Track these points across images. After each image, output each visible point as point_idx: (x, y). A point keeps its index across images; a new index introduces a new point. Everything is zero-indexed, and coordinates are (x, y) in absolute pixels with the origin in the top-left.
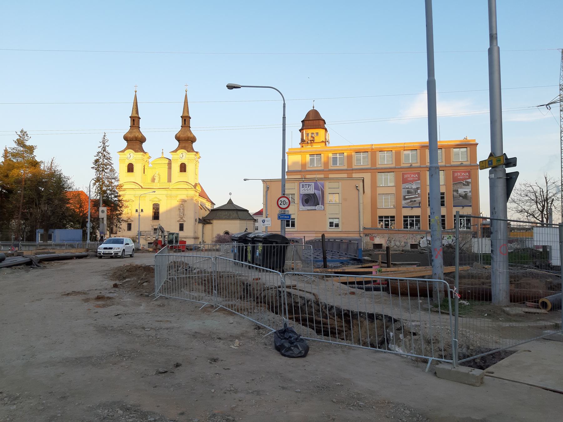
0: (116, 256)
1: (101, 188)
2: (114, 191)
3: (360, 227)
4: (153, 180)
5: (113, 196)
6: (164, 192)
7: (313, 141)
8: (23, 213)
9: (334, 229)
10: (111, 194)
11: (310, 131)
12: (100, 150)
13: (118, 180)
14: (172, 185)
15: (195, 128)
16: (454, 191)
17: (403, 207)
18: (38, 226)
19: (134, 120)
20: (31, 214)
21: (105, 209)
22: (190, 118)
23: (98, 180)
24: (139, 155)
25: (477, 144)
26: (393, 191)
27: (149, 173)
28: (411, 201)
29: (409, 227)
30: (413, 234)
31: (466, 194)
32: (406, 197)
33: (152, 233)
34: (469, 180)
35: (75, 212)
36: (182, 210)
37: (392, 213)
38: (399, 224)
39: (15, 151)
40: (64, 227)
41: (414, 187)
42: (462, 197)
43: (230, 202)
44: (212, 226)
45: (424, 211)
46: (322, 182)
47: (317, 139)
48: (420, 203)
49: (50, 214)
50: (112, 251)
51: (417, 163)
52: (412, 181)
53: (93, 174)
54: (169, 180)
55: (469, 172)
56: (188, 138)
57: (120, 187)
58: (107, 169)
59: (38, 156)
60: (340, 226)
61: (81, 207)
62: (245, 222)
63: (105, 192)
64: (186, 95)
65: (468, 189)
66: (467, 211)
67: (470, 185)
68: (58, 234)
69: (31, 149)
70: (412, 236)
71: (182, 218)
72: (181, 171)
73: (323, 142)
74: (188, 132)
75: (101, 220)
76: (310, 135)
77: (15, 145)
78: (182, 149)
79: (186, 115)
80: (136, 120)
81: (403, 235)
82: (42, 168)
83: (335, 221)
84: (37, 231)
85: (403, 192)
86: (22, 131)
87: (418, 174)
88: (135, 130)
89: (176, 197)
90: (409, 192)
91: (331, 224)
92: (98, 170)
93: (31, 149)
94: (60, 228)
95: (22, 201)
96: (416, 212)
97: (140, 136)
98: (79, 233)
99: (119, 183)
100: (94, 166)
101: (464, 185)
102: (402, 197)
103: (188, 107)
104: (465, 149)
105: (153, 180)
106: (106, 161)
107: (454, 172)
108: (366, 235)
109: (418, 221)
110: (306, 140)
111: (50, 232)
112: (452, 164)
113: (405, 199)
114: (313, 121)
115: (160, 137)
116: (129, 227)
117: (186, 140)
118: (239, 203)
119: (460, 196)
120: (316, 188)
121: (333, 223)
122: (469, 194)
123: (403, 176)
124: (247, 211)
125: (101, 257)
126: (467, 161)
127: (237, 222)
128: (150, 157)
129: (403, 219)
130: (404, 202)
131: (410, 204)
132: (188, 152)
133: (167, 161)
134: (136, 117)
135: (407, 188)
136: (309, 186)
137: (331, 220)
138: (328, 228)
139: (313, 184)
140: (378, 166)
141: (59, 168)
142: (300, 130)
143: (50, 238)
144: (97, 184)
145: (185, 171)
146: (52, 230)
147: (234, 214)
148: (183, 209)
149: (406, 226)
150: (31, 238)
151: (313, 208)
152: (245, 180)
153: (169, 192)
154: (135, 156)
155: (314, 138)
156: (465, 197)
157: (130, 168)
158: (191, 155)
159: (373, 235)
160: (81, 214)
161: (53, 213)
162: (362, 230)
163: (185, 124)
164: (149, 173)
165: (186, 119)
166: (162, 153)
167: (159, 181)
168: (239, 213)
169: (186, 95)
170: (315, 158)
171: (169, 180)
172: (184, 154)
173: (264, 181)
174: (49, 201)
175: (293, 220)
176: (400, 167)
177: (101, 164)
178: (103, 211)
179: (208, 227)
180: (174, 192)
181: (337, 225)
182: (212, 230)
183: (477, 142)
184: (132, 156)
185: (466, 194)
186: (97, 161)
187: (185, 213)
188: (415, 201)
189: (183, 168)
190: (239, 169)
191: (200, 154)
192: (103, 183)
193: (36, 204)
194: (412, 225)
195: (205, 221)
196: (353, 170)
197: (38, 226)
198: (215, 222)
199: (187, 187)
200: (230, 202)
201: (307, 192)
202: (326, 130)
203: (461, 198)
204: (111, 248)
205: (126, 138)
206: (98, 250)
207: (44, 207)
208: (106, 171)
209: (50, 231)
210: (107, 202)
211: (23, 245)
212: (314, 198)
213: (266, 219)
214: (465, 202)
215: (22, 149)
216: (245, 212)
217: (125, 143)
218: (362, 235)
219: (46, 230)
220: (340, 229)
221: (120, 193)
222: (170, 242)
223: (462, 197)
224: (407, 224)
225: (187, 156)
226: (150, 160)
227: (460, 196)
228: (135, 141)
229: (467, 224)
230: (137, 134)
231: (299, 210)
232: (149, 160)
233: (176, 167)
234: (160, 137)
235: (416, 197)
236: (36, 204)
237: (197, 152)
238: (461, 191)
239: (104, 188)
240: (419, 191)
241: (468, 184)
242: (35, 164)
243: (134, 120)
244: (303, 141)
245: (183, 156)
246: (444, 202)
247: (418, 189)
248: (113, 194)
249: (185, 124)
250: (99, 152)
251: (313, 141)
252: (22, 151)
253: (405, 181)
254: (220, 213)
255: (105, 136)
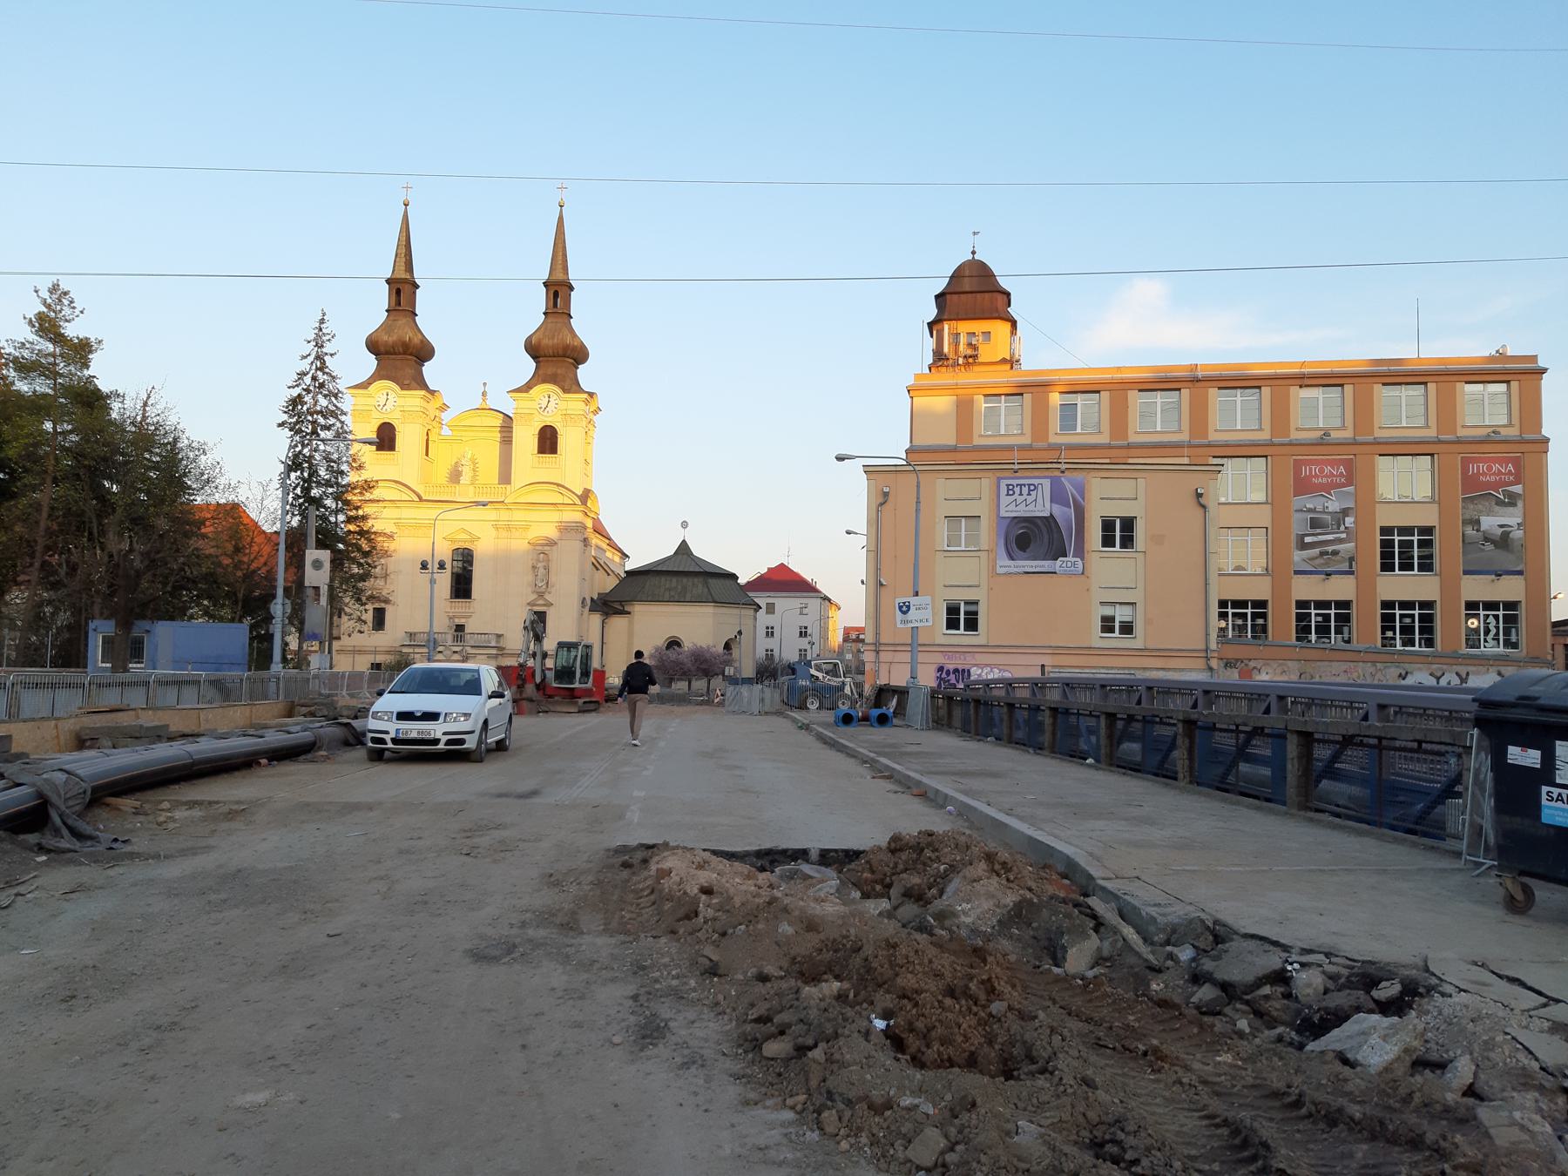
0: (455, 754)
1: (307, 490)
2: (346, 503)
3: (1207, 634)
4: (455, 476)
5: (341, 518)
6: (489, 514)
7: (972, 360)
8: (44, 564)
9: (1116, 640)
10: (337, 512)
11: (964, 327)
12: (304, 365)
13: (360, 467)
14: (512, 493)
15: (585, 322)
16: (1465, 522)
17: (1296, 572)
18: (97, 609)
19: (398, 292)
20: (73, 569)
21: (325, 555)
22: (572, 288)
23: (294, 464)
24: (414, 398)
25: (1544, 371)
26: (1264, 517)
27: (444, 458)
28: (1322, 554)
29: (1313, 637)
30: (1374, 663)
31: (1505, 535)
32: (1308, 540)
33: (450, 638)
34: (1517, 489)
35: (219, 564)
36: (541, 571)
37: (1259, 590)
38: (1282, 624)
39: (26, 354)
40: (176, 613)
41: (1334, 506)
42: (1493, 542)
43: (684, 548)
44: (631, 623)
45: (1365, 588)
46: (1078, 476)
47: (985, 354)
48: (1351, 560)
49: (138, 564)
50: (437, 730)
51: (1343, 428)
52: (1328, 488)
53: (281, 444)
54: (505, 478)
55: (1517, 462)
56: (566, 348)
57: (368, 486)
58: (328, 428)
59: (104, 373)
60: (1139, 628)
61: (237, 550)
62: (736, 611)
63: (317, 502)
64: (561, 219)
65: (1511, 517)
66: (1509, 589)
67: (1520, 504)
68: (164, 636)
69: (81, 351)
70: (1372, 670)
71: (541, 595)
72: (542, 450)
73: (1004, 361)
74: (566, 332)
75: (310, 592)
76: (963, 340)
77: (27, 334)
78: (544, 381)
79: (560, 276)
80: (406, 289)
81: (1344, 666)
82: (114, 415)
83: (1122, 614)
84: (92, 625)
85: (1298, 524)
86: (54, 289)
87: (1349, 465)
88: (403, 321)
89: (526, 528)
90: (1315, 524)
91: (1108, 625)
92: (295, 429)
93: (81, 351)
94: (172, 619)
95: (43, 525)
96: (1340, 588)
97: (416, 340)
98: (236, 635)
99: (365, 475)
100: (285, 417)
101: (1500, 503)
102: (1293, 538)
103: (565, 255)
104: (1502, 387)
105: (455, 476)
106: (323, 402)
107: (1466, 462)
108: (1229, 664)
109: (1344, 619)
110: (951, 356)
111: (136, 633)
112: (1461, 433)
113: (1303, 546)
114: (973, 295)
115: (480, 346)
116: (379, 621)
117: (556, 357)
118: (709, 551)
119: (1486, 539)
120: (1058, 496)
121: (1112, 619)
122: (1517, 534)
123: (1297, 472)
124: (734, 577)
125: (378, 756)
126: (1510, 425)
127: (707, 610)
128: (444, 408)
129: (1294, 611)
130: (1298, 556)
131: (1320, 561)
132: (565, 391)
133: (498, 421)
134: (405, 281)
135: (1310, 510)
136: (1032, 488)
137: (1108, 611)
138: (1096, 638)
139: (1047, 483)
140: (1213, 437)
141: (172, 420)
142: (931, 325)
143: (136, 651)
144: (293, 475)
145: (553, 450)
146: (146, 624)
147: (698, 586)
148: (547, 568)
149: (1303, 631)
150: (71, 655)
151: (1046, 565)
152: (840, 458)
153: (504, 515)
154: (400, 402)
155: (975, 348)
156: (1503, 541)
157: (386, 439)
158: (574, 403)
159: (1252, 664)
160: (239, 574)
161: (152, 562)
162: (1213, 646)
163: (555, 305)
164: (444, 458)
165: (558, 291)
166: (484, 394)
167: (474, 477)
168: (712, 582)
169: (561, 219)
170: (1003, 405)
171: (505, 478)
172: (554, 397)
173: (869, 471)
174: (138, 522)
175: (972, 608)
176: (1286, 440)
177: (308, 414)
178: (317, 565)
179: (618, 622)
180: (519, 516)
181: (1127, 628)
182: (631, 634)
183: (1541, 363)
184: (390, 401)
185: (1505, 535)
186: (296, 402)
187: (553, 579)
188: (1335, 553)
189: (548, 441)
190: (755, 441)
191: (601, 400)
192: (313, 472)
193: (91, 533)
194: (1323, 630)
195: (608, 605)
196: (1129, 446)
197: (97, 609)
198: (638, 609)
199: (559, 499)
200: (684, 548)
201: (1022, 511)
202: (1014, 323)
203: (1489, 547)
204: (432, 716)
205: (373, 346)
206: (372, 724)
207: (117, 543)
208: (323, 434)
209: (139, 627)
210: (326, 538)
211: (26, 685)
212: (1050, 531)
213: (914, 601)
214: (1504, 559)
215: (50, 347)
216: (728, 582)
217: (530, 365)
218: (1214, 663)
219: (125, 624)
220: (1137, 641)
221: (368, 509)
222: (565, 674)
223: (1493, 542)
224: (1307, 630)
225: (563, 405)
226: (446, 417)
227: (1486, 539)
228: (401, 355)
229: (1507, 632)
230: (408, 335)
231: (993, 573)
232: (443, 415)
233: (525, 439)
234: (480, 346)
235: (1341, 541)
236: (91, 533)
237: (591, 395)
238: (1490, 523)
239: (315, 492)
240: (1349, 521)
241: (1512, 500)
242: (91, 400)
243: (398, 292)
244: (939, 358)
245: (548, 404)
246: (1431, 557)
247: (1345, 512)
248: (341, 510)
249: (555, 305)
250: (302, 374)
251: (972, 360)
252: (54, 355)
253: (1303, 486)
254: (652, 581)
255: (322, 321)
